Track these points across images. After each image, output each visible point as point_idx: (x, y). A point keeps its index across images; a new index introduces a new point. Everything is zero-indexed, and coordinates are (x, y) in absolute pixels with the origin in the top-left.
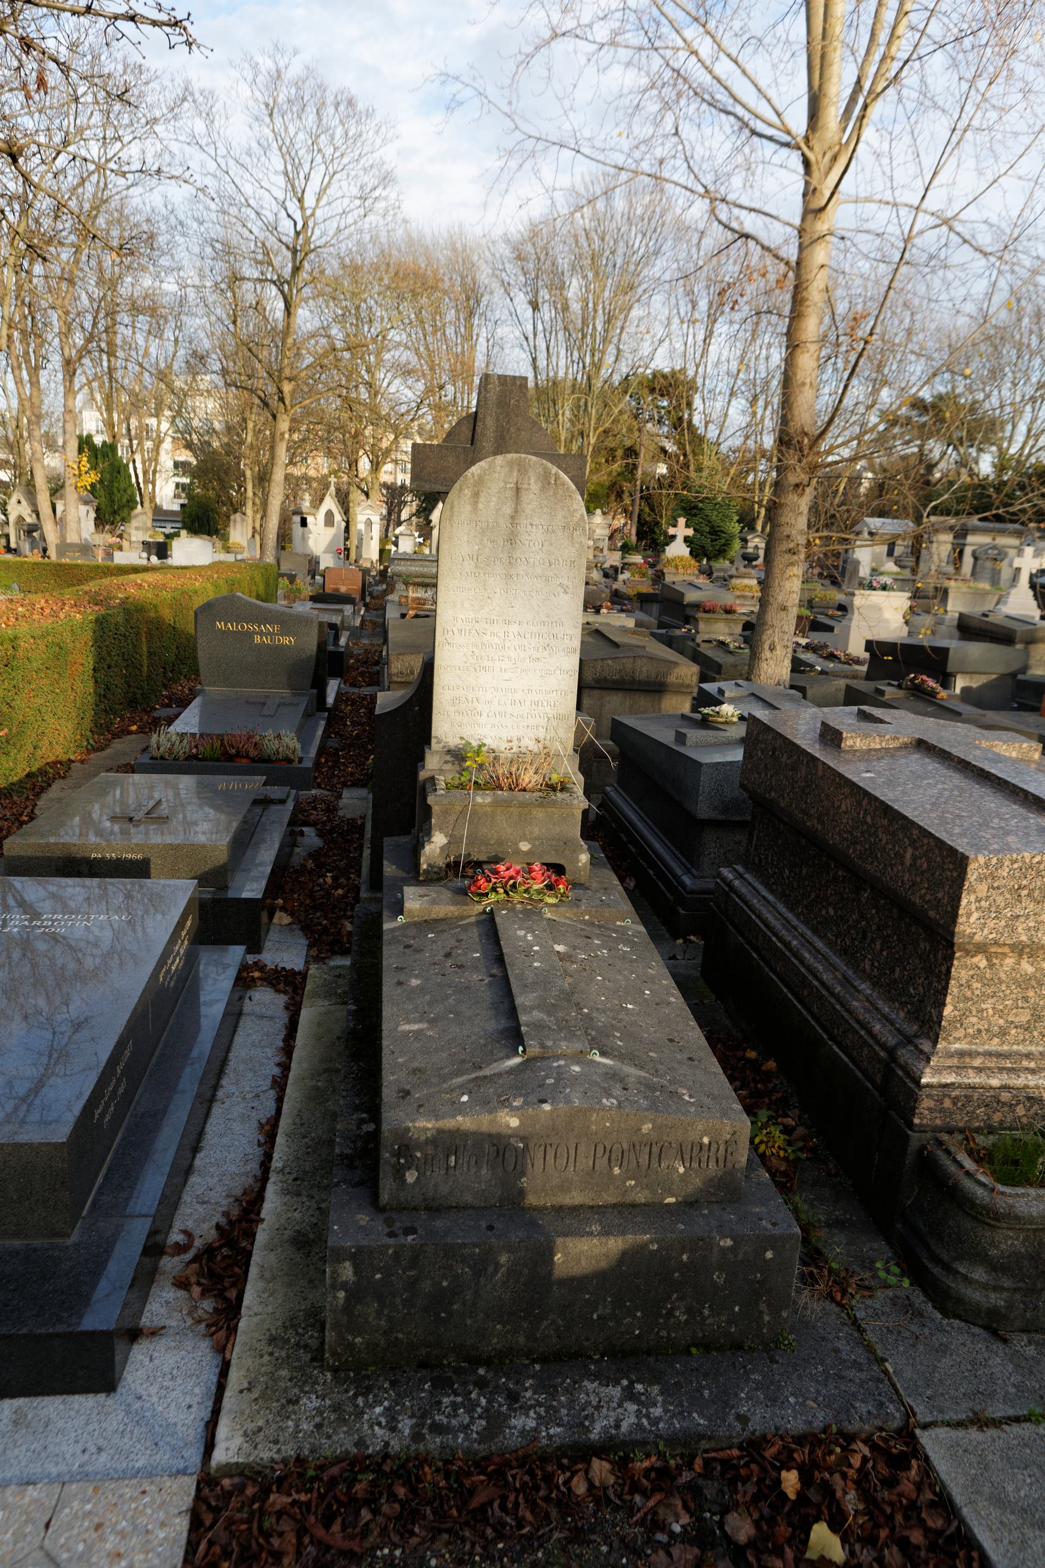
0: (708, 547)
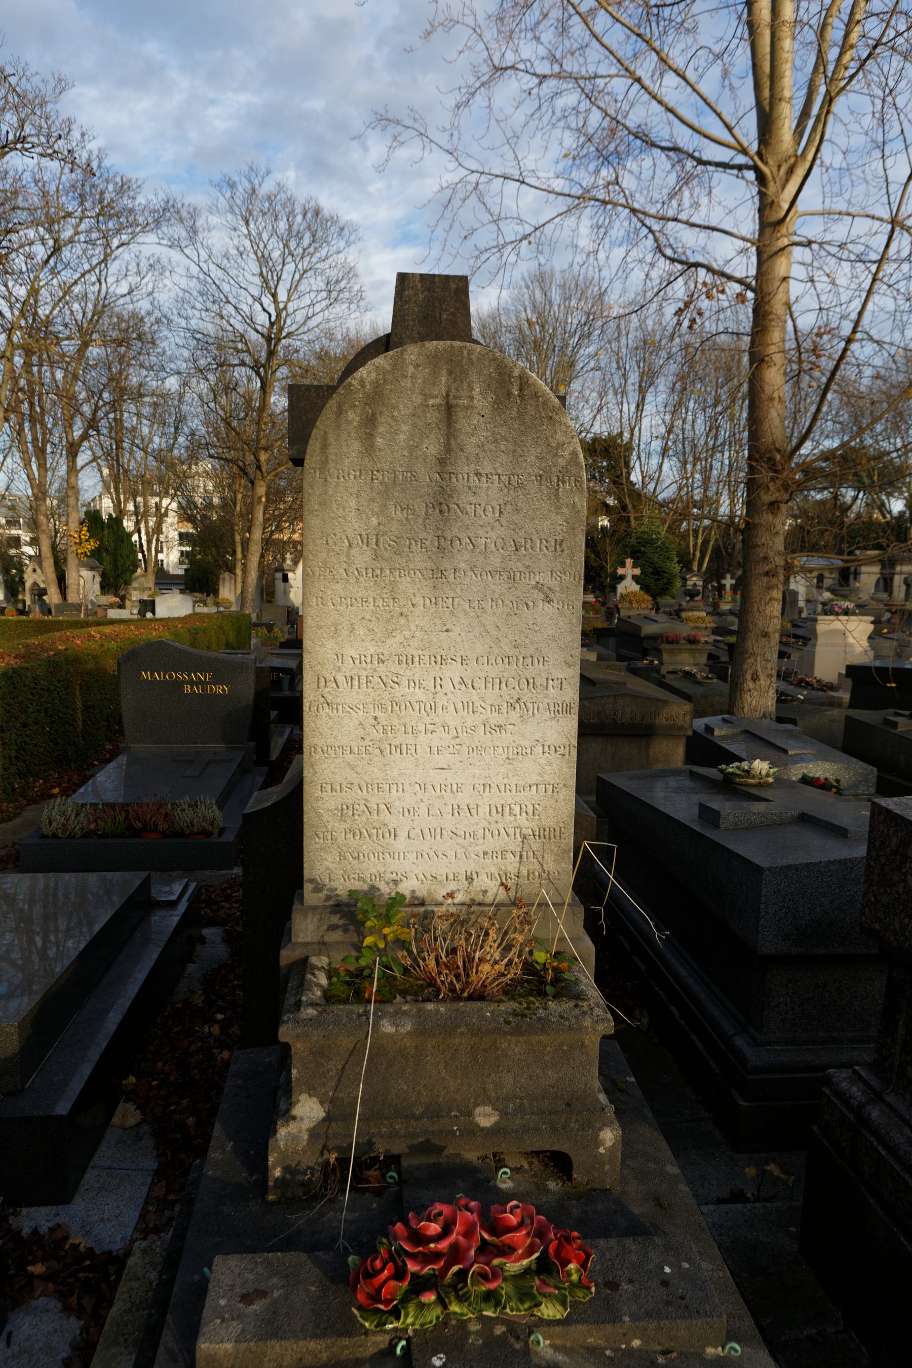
0: (655, 583)
